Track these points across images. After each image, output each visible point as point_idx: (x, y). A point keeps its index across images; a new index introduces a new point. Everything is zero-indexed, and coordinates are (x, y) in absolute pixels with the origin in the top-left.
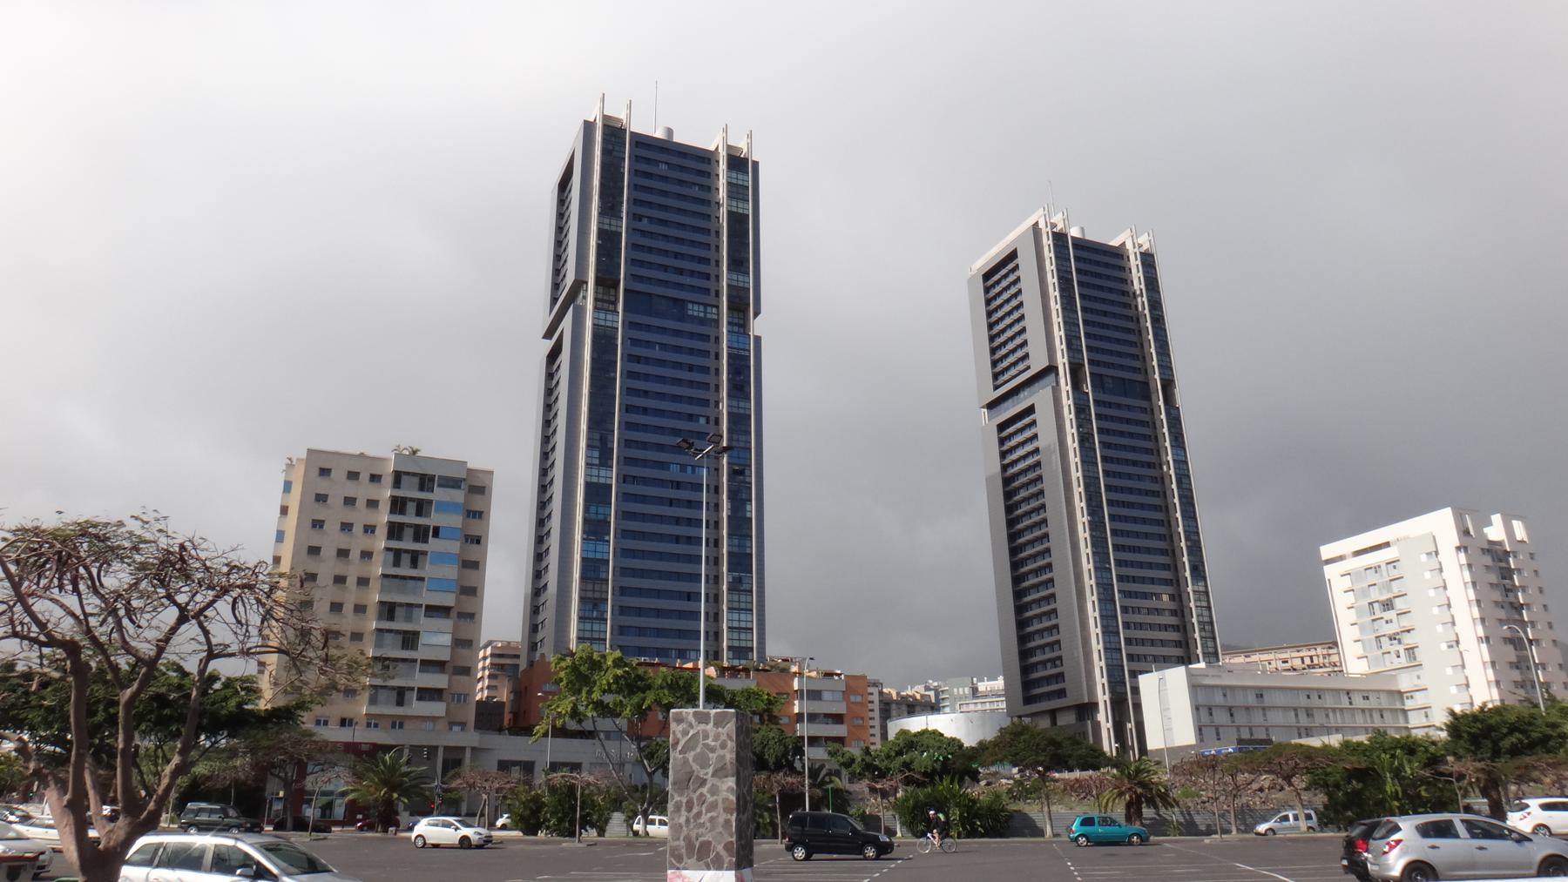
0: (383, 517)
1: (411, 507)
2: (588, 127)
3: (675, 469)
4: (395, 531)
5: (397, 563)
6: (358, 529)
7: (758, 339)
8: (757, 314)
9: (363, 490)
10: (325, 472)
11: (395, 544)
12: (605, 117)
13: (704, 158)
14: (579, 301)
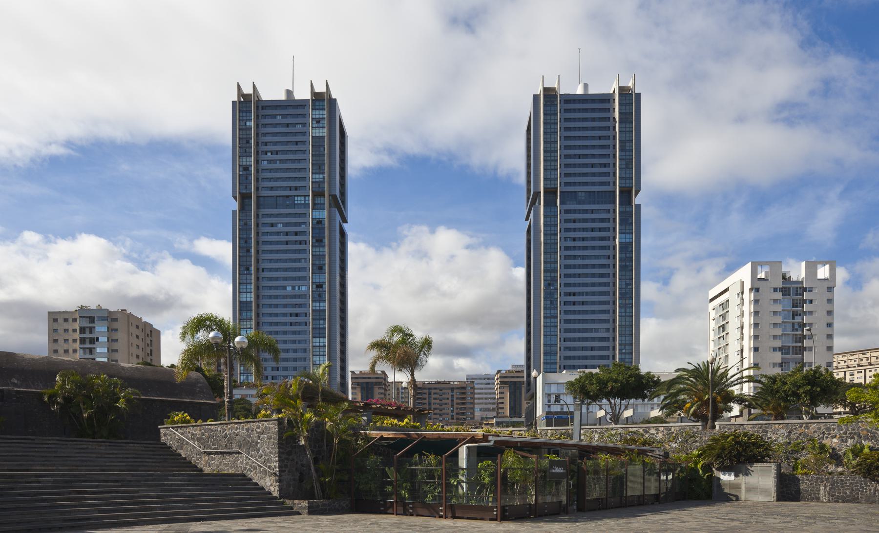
0: (77, 336)
1: (87, 331)
2: (536, 98)
3: (289, 288)
4: (83, 340)
5: (85, 353)
6: (70, 341)
7: (638, 207)
8: (637, 192)
9: (71, 326)
10: (55, 320)
11: (83, 346)
12: (545, 89)
13: (605, 99)
14: (537, 204)
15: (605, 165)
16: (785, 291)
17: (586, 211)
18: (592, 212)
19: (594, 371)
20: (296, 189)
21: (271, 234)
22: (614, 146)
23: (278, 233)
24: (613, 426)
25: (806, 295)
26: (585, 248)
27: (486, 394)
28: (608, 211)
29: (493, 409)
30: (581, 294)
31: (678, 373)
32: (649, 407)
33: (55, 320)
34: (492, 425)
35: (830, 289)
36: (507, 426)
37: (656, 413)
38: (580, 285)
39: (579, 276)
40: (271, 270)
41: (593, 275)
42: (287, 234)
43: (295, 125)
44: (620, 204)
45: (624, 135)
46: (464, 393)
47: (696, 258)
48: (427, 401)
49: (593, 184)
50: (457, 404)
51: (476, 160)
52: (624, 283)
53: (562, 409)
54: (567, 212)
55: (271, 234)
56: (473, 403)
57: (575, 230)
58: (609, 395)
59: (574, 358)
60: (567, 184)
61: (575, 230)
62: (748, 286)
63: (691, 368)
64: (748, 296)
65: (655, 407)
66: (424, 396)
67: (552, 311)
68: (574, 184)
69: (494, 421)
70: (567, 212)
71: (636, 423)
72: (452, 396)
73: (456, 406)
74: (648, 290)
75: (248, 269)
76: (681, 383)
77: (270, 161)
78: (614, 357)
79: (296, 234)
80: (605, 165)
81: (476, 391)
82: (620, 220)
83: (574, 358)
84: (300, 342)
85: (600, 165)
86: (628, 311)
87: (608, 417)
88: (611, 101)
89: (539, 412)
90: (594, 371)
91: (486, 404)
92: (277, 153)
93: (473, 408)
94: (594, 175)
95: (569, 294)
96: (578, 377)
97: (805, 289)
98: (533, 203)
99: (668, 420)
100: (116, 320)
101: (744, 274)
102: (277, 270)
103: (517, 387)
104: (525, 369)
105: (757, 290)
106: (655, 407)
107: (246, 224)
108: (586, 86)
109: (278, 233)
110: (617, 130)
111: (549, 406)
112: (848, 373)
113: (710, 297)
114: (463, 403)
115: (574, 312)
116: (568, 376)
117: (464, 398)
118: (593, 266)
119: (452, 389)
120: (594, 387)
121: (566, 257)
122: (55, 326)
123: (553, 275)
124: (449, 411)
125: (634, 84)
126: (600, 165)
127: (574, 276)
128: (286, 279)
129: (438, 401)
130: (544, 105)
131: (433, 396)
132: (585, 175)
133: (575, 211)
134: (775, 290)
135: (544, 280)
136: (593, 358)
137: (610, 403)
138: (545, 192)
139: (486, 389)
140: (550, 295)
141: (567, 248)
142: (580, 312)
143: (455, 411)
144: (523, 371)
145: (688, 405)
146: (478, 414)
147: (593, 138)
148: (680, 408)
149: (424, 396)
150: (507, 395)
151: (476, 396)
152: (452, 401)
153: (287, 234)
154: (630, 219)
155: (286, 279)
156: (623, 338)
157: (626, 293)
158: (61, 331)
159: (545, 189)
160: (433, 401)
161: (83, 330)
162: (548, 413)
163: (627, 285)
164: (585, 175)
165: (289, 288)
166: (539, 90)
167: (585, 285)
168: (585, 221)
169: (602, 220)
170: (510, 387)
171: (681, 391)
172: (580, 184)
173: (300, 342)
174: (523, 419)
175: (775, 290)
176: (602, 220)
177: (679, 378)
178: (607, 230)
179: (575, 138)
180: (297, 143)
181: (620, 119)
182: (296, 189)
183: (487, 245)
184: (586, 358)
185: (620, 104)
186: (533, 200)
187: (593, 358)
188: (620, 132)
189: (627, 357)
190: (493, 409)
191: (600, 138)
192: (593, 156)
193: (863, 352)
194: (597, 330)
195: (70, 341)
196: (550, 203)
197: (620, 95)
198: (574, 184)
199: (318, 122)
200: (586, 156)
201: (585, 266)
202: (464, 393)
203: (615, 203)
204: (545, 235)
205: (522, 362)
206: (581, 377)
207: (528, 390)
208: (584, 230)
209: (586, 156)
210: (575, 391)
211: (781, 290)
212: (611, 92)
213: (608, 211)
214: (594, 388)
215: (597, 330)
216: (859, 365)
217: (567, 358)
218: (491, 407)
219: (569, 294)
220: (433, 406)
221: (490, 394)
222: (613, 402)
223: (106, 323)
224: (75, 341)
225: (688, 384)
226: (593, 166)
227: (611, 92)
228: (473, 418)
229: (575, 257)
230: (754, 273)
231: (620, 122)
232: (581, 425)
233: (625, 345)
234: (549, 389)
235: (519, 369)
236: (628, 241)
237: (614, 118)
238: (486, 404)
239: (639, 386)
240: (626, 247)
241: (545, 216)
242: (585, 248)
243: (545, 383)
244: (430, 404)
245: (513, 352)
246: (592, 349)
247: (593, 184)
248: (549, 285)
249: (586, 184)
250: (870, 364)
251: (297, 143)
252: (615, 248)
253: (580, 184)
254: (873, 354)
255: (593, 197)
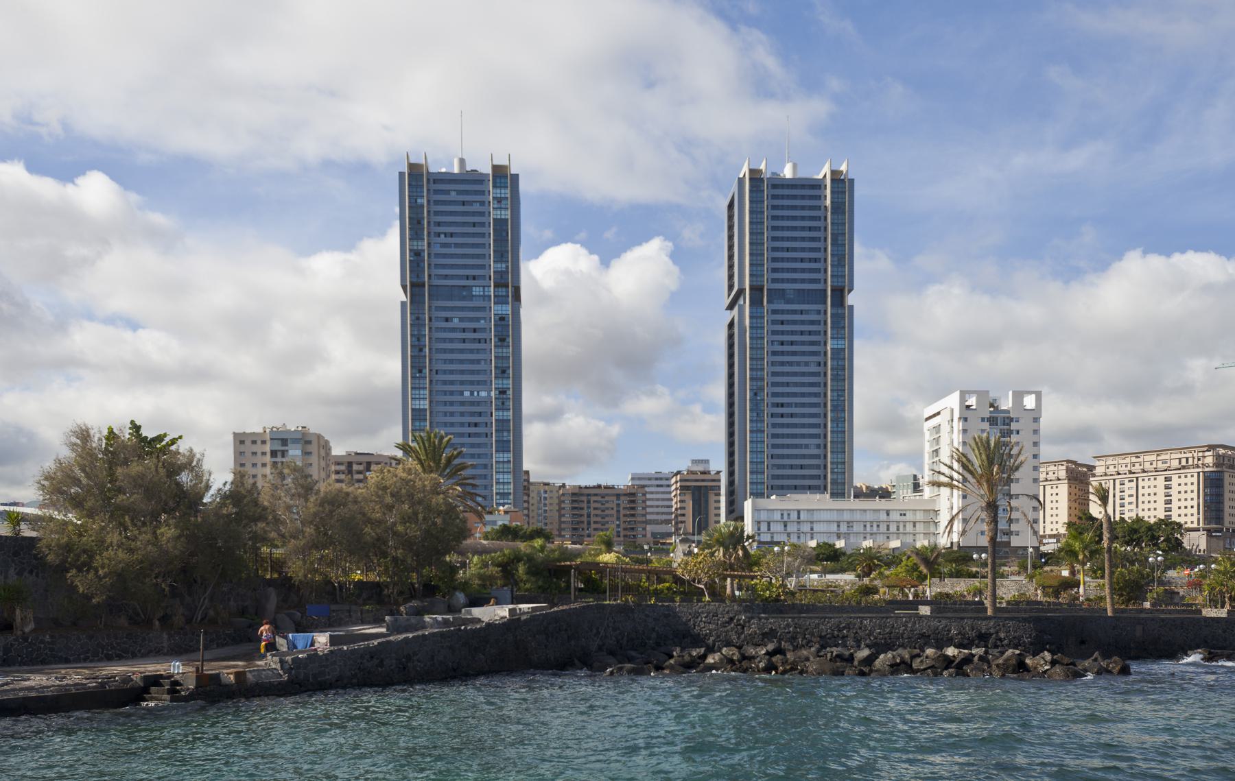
1: (279, 454)
3: (467, 394)
7: (851, 308)
9: (258, 448)
10: (242, 442)
13: (818, 185)
15: (816, 260)
16: (992, 421)
17: (794, 312)
20: (474, 278)
21: (445, 330)
22: (826, 239)
23: (453, 330)
25: (1014, 426)
30: (789, 405)
33: (242, 442)
35: (1036, 420)
39: (788, 384)
40: (445, 372)
42: (464, 330)
43: (471, 203)
46: (633, 502)
48: (585, 512)
49: (803, 281)
54: (774, 312)
55: (445, 330)
57: (783, 333)
60: (774, 281)
61: (783, 333)
62: (957, 415)
64: (958, 426)
66: (582, 505)
68: (783, 281)
70: (774, 312)
72: (618, 505)
73: (623, 519)
75: (420, 371)
77: (444, 245)
79: (475, 330)
80: (816, 260)
84: (479, 456)
85: (810, 260)
92: (452, 235)
94: (803, 271)
95: (777, 405)
97: (1012, 420)
100: (309, 442)
101: (952, 401)
102: (452, 372)
105: (966, 419)
107: (418, 318)
109: (453, 330)
112: (1117, 482)
113: (926, 416)
114: (633, 515)
115: (782, 426)
117: (633, 508)
119: (618, 496)
122: (242, 448)
124: (614, 526)
126: (810, 260)
128: (462, 383)
129: (599, 512)
131: (593, 505)
134: (983, 420)
139: (657, 493)
142: (788, 426)
143: (623, 526)
149: (582, 505)
150: (689, 505)
152: (618, 511)
153: (464, 330)
155: (462, 383)
158: (248, 454)
160: (593, 512)
161: (274, 453)
164: (794, 270)
165: (467, 394)
167: (795, 395)
169: (812, 323)
173: (479, 456)
175: (983, 420)
176: (812, 323)
179: (782, 239)
180: (474, 225)
182: (474, 278)
185: (832, 192)
191: (810, 229)
192: (803, 250)
193: (1137, 455)
194: (807, 446)
195: (259, 465)
196: (756, 302)
197: (832, 180)
198: (783, 281)
199: (499, 202)
200: (795, 250)
202: (633, 502)
203: (825, 303)
209: (795, 250)
211: (989, 420)
215: (807, 446)
216: (1131, 472)
219: (777, 405)
220: (593, 519)
223: (300, 446)
224: (264, 465)
226: (802, 260)
227: (820, 176)
230: (963, 399)
243: (755, 510)
244: (589, 516)
247: (803, 281)
249: (794, 281)
250: (1144, 471)
251: (474, 225)
252: (825, 353)
254: (1147, 458)
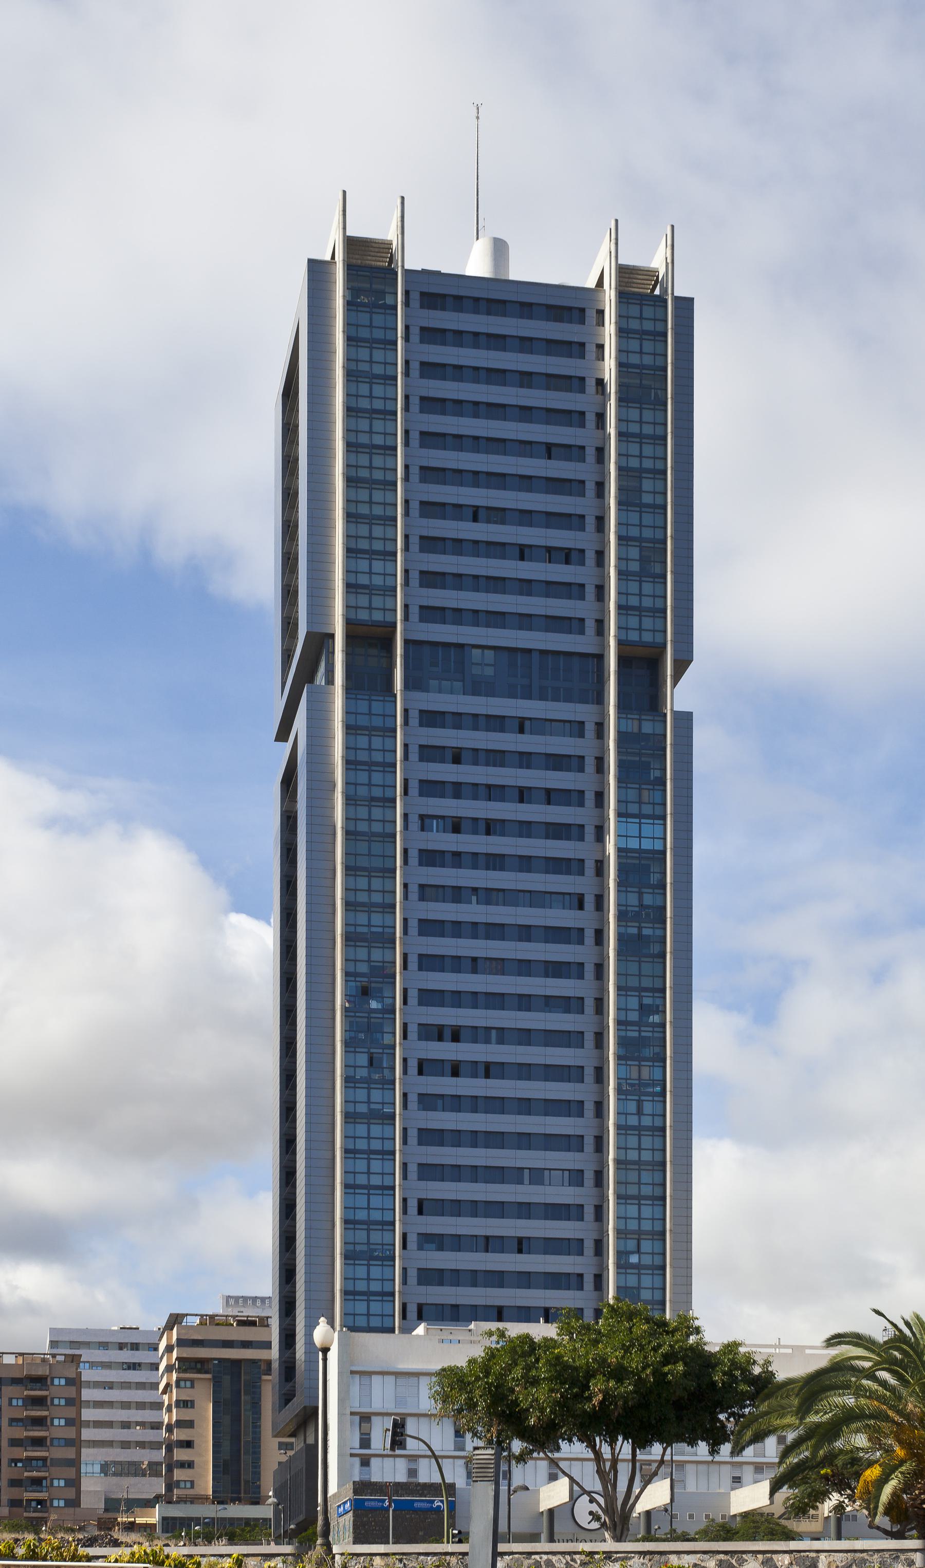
2: (318, 271)
7: (685, 720)
12: (353, 245)
13: (567, 307)
14: (320, 679)
15: (568, 556)
17: (497, 723)
18: (521, 725)
19: (541, 1331)
24: (610, 1545)
26: (496, 862)
27: (126, 1405)
28: (577, 729)
29: (153, 1469)
30: (480, 1034)
31: (834, 1352)
32: (727, 1473)
34: (148, 1529)
36: (209, 1539)
37: (753, 1496)
38: (475, 1000)
39: (475, 965)
41: (525, 967)
44: (622, 707)
45: (634, 449)
46: (39, 1402)
47: (868, 927)
49: (525, 621)
50: (14, 1443)
51: (70, 492)
52: (633, 1003)
53: (413, 1473)
54: (430, 718)
56: (76, 1443)
57: (457, 790)
58: (593, 1425)
59: (455, 1277)
60: (430, 614)
61: (457, 790)
63: (879, 1332)
65: (748, 1473)
67: (376, 1095)
68: (458, 616)
69: (154, 1517)
70: (430, 718)
71: (685, 1538)
74: (714, 1039)
76: (846, 1386)
78: (599, 1281)
80: (568, 556)
81: (87, 1394)
82: (620, 764)
83: (455, 1277)
85: (551, 554)
86: (648, 1108)
87: (583, 1507)
88: (591, 315)
89: (335, 1483)
90: (541, 1331)
91: (125, 1445)
93: (75, 1463)
94: (526, 587)
95: (438, 1033)
96: (478, 1352)
98: (306, 674)
99: (794, 1525)
103: (243, 1380)
104: (273, 1314)
106: (748, 1473)
108: (500, 249)
110: (612, 428)
111: (365, 1462)
114: (38, 1442)
115: (456, 1103)
116: (463, 1347)
117: (39, 1422)
118: (525, 933)
120: (541, 1394)
121: (426, 892)
123: (377, 955)
125: (671, 264)
126: (551, 554)
127: (456, 964)
130: (350, 305)
132: (497, 584)
133: (458, 720)
135: (347, 974)
136: (525, 1280)
137: (598, 1456)
138: (350, 638)
140: (367, 1033)
141: (430, 858)
142: (475, 1104)
144: (263, 1322)
145: (873, 1473)
146: (94, 1487)
147: (525, 447)
148: (841, 1483)
151: (87, 1414)
154: (655, 762)
156: (632, 1210)
157: (641, 1042)
159: (349, 623)
162: (361, 1487)
163: (645, 1010)
164: (497, 584)
166: (328, 246)
167: (497, 1001)
168: (496, 758)
169: (557, 762)
170: (217, 1384)
171: (848, 1417)
172: (477, 617)
174: (265, 1511)
176: (557, 762)
177: (838, 1367)
178: (573, 797)
181: (621, 386)
183: (126, 819)
184: (497, 1279)
185: (622, 332)
186: (305, 665)
187: (525, 1280)
188: (620, 434)
189: (647, 1281)
190: (153, 1469)
191: (550, 450)
194: (537, 1176)
196: (367, 682)
197: (623, 296)
198: (458, 616)
200: (498, 515)
201: (495, 931)
202: (39, 1402)
203: (600, 699)
204: (350, 800)
205: (264, 1283)
206: (492, 1355)
207: (287, 1398)
208: (493, 792)
210: (471, 1405)
212: (591, 283)
213: (577, 729)
214: (538, 1400)
215: (537, 1176)
217: (429, 1277)
218: (145, 1457)
221: (141, 1406)
222: (606, 1450)
225: (872, 1395)
226: (523, 552)
228: (74, 1503)
229: (457, 894)
231: (620, 400)
232: (496, 1540)
233: (639, 1235)
234: (367, 1393)
235: (251, 1312)
236: (647, 845)
237: (600, 383)
238: (125, 1445)
239: (692, 1395)
240: (641, 869)
241: (350, 729)
242: (496, 862)
243: (355, 1373)
245: (227, 1247)
246: (521, 1245)
247: (525, 621)
248: (365, 992)
249: (497, 619)
252: (600, 867)
253: (477, 617)
255: (530, 672)
